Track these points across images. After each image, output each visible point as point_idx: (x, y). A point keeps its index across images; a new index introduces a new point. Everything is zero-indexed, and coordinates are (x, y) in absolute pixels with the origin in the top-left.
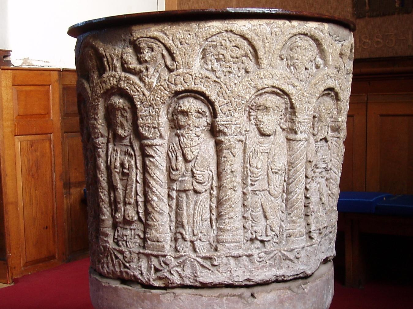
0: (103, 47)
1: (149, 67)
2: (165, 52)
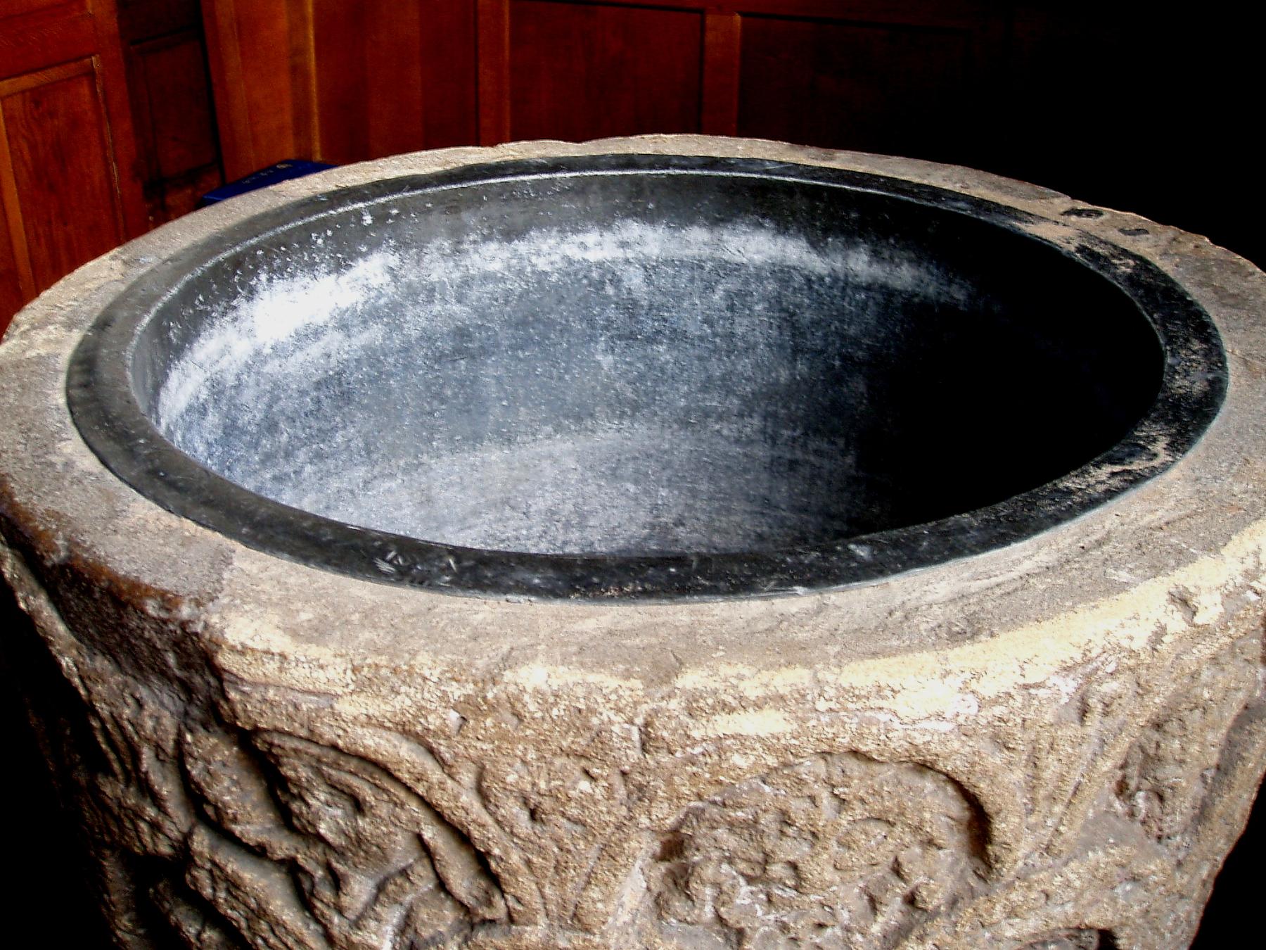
0: (75, 652)
1: (344, 875)
2: (430, 833)
